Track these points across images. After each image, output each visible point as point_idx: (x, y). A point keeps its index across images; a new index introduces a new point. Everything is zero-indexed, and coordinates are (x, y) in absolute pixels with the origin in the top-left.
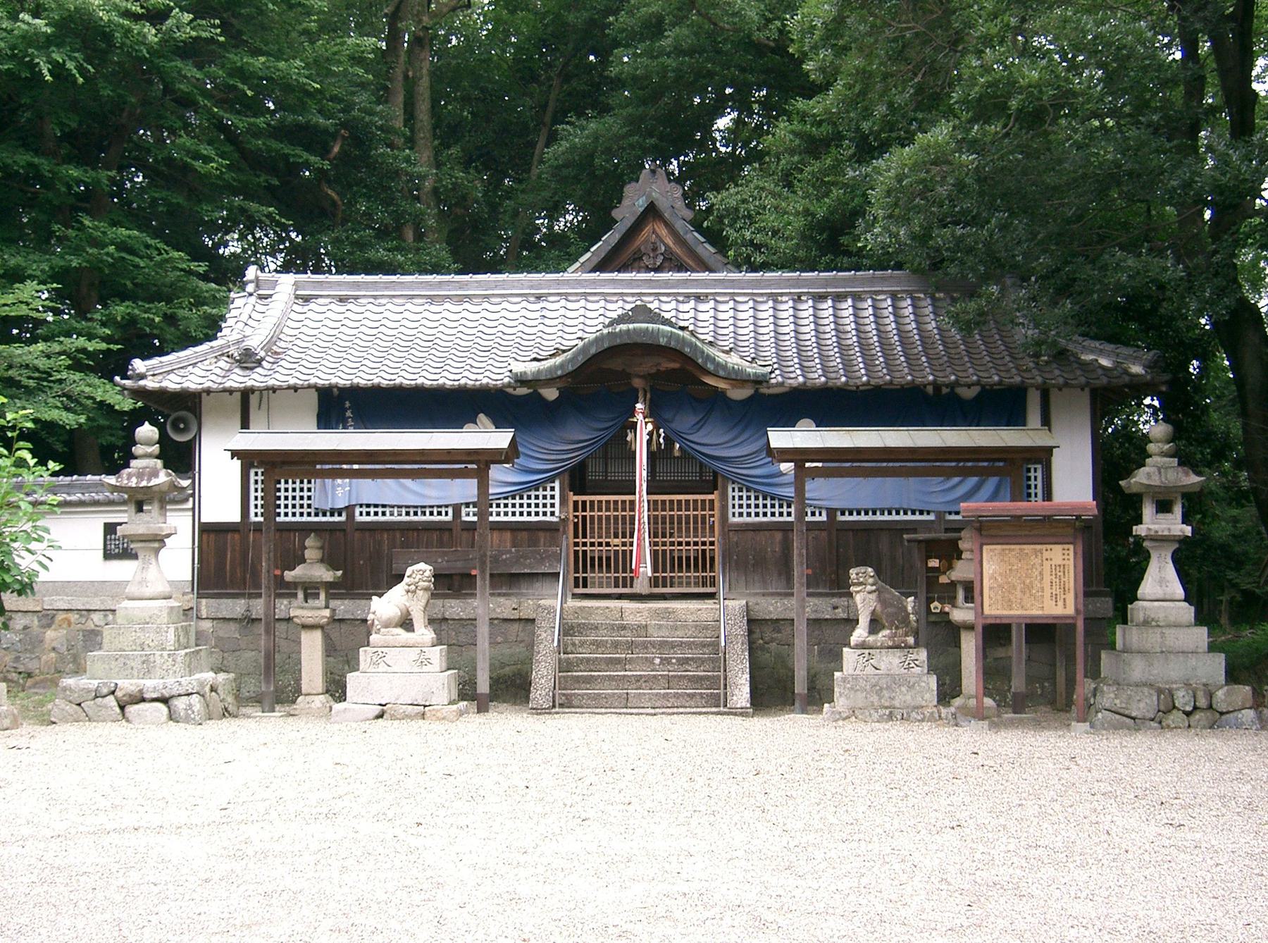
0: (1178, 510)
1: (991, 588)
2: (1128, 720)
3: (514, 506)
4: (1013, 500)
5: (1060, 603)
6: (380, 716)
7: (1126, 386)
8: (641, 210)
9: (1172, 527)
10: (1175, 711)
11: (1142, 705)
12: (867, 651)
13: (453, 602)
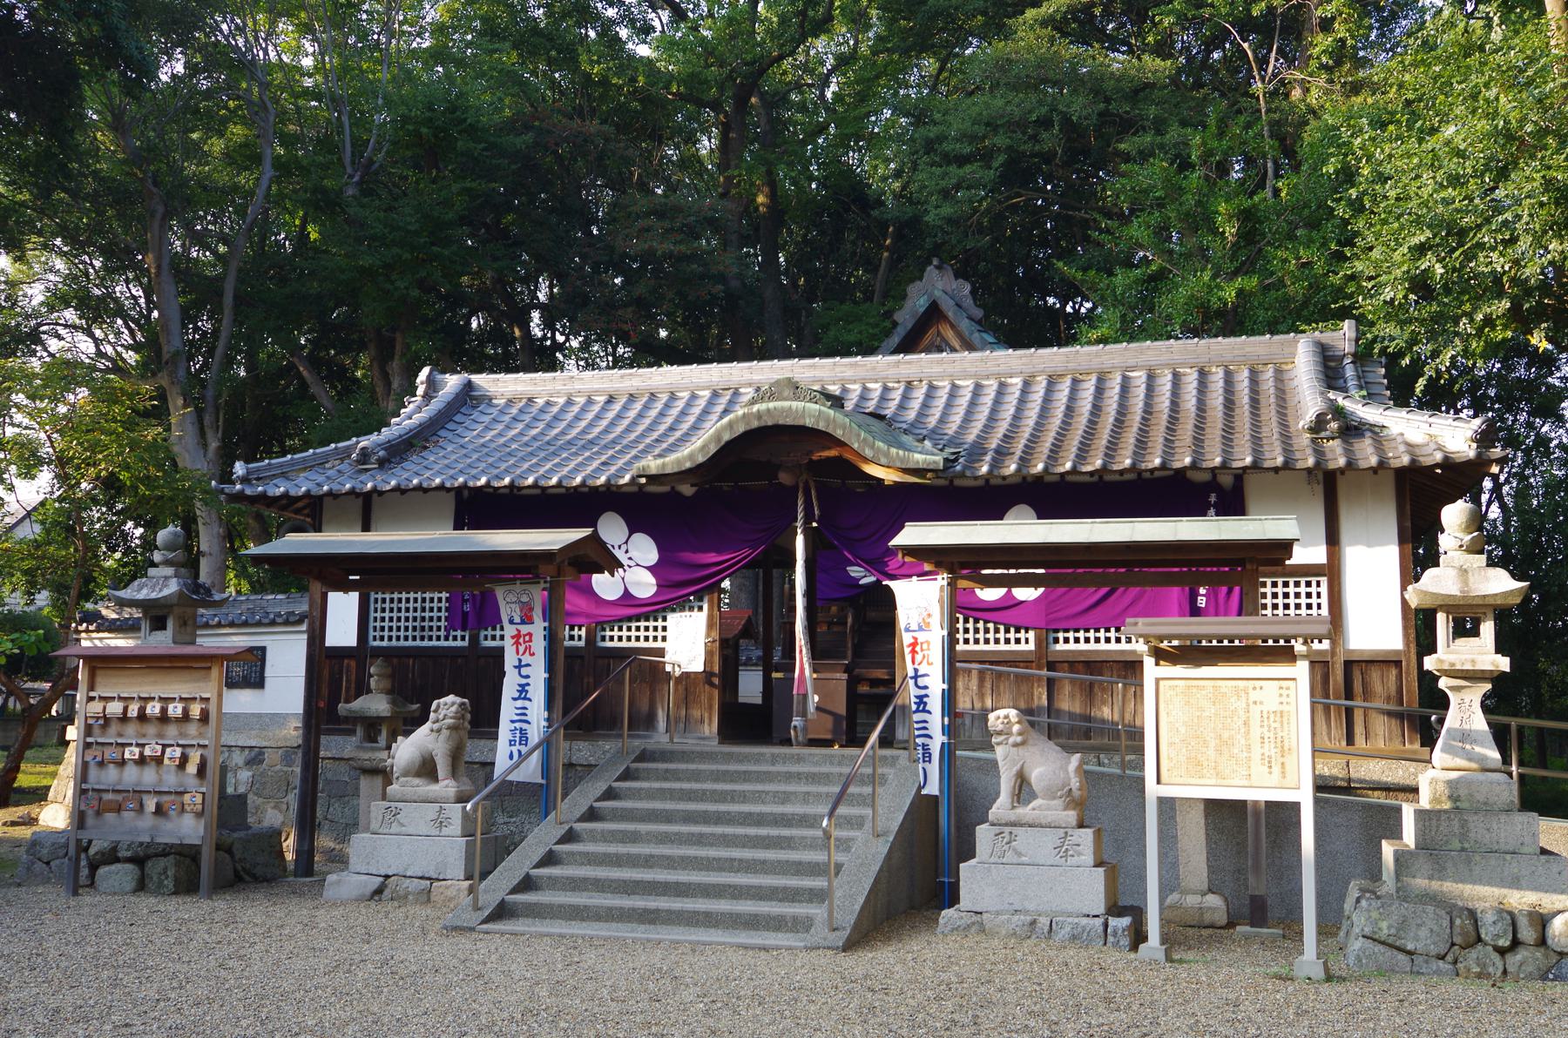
0: (1488, 628)
1: (1171, 744)
2: (1401, 957)
3: (647, 629)
4: (458, 526)
5: (1276, 769)
6: (379, 891)
7: (1437, 465)
8: (922, 310)
9: (1479, 658)
10: (1479, 947)
11: (1424, 932)
12: (1007, 829)
13: (581, 744)
